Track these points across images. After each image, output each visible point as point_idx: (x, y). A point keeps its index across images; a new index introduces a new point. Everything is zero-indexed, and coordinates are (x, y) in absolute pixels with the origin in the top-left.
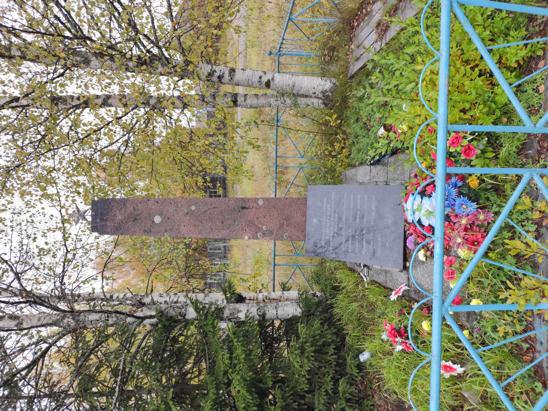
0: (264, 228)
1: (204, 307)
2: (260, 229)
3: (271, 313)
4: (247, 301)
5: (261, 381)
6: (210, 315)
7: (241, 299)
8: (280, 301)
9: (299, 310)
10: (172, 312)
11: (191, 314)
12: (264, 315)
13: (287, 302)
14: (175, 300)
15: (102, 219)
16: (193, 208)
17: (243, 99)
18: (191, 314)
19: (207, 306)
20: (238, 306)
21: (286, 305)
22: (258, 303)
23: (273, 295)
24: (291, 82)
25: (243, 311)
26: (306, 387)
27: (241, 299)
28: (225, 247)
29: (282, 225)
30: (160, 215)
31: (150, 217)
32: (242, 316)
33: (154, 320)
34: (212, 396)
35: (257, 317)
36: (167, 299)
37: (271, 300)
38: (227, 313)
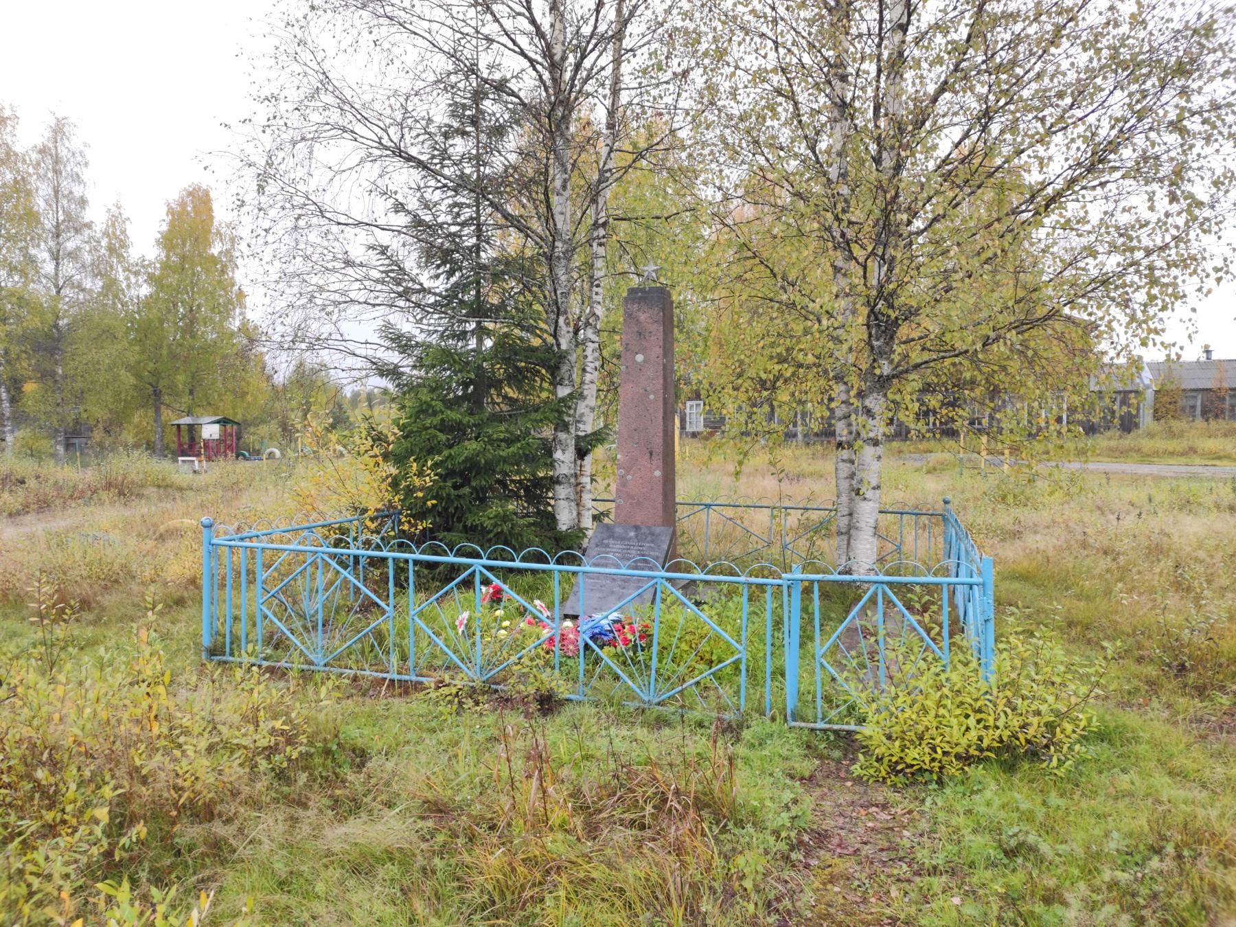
0: (629, 477)
1: (570, 408)
2: (628, 472)
3: (562, 491)
4: (579, 462)
5: (478, 473)
6: (560, 413)
7: (581, 453)
8: (578, 505)
9: (564, 528)
10: (564, 368)
11: (563, 392)
12: (558, 482)
13: (575, 514)
14: (588, 369)
15: (640, 298)
16: (652, 397)
17: (845, 457)
18: (563, 392)
19: (572, 412)
20: (571, 450)
21: (571, 512)
22: (576, 476)
23: (587, 498)
24: (862, 525)
25: (564, 458)
26: (469, 523)
27: (581, 453)
28: (795, 435)
29: (632, 497)
30: (644, 361)
31: (643, 350)
32: (558, 455)
33: (555, 348)
34: (466, 420)
35: (557, 474)
36: (590, 359)
37: (579, 494)
38: (562, 436)
